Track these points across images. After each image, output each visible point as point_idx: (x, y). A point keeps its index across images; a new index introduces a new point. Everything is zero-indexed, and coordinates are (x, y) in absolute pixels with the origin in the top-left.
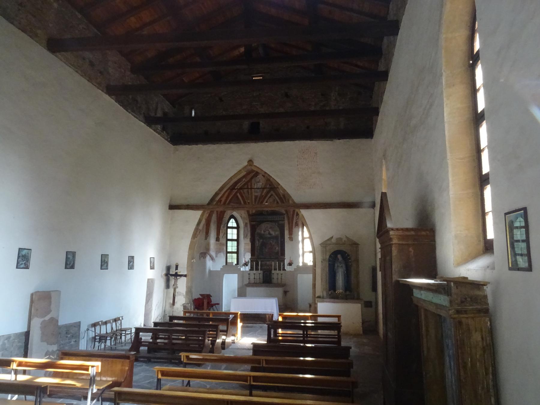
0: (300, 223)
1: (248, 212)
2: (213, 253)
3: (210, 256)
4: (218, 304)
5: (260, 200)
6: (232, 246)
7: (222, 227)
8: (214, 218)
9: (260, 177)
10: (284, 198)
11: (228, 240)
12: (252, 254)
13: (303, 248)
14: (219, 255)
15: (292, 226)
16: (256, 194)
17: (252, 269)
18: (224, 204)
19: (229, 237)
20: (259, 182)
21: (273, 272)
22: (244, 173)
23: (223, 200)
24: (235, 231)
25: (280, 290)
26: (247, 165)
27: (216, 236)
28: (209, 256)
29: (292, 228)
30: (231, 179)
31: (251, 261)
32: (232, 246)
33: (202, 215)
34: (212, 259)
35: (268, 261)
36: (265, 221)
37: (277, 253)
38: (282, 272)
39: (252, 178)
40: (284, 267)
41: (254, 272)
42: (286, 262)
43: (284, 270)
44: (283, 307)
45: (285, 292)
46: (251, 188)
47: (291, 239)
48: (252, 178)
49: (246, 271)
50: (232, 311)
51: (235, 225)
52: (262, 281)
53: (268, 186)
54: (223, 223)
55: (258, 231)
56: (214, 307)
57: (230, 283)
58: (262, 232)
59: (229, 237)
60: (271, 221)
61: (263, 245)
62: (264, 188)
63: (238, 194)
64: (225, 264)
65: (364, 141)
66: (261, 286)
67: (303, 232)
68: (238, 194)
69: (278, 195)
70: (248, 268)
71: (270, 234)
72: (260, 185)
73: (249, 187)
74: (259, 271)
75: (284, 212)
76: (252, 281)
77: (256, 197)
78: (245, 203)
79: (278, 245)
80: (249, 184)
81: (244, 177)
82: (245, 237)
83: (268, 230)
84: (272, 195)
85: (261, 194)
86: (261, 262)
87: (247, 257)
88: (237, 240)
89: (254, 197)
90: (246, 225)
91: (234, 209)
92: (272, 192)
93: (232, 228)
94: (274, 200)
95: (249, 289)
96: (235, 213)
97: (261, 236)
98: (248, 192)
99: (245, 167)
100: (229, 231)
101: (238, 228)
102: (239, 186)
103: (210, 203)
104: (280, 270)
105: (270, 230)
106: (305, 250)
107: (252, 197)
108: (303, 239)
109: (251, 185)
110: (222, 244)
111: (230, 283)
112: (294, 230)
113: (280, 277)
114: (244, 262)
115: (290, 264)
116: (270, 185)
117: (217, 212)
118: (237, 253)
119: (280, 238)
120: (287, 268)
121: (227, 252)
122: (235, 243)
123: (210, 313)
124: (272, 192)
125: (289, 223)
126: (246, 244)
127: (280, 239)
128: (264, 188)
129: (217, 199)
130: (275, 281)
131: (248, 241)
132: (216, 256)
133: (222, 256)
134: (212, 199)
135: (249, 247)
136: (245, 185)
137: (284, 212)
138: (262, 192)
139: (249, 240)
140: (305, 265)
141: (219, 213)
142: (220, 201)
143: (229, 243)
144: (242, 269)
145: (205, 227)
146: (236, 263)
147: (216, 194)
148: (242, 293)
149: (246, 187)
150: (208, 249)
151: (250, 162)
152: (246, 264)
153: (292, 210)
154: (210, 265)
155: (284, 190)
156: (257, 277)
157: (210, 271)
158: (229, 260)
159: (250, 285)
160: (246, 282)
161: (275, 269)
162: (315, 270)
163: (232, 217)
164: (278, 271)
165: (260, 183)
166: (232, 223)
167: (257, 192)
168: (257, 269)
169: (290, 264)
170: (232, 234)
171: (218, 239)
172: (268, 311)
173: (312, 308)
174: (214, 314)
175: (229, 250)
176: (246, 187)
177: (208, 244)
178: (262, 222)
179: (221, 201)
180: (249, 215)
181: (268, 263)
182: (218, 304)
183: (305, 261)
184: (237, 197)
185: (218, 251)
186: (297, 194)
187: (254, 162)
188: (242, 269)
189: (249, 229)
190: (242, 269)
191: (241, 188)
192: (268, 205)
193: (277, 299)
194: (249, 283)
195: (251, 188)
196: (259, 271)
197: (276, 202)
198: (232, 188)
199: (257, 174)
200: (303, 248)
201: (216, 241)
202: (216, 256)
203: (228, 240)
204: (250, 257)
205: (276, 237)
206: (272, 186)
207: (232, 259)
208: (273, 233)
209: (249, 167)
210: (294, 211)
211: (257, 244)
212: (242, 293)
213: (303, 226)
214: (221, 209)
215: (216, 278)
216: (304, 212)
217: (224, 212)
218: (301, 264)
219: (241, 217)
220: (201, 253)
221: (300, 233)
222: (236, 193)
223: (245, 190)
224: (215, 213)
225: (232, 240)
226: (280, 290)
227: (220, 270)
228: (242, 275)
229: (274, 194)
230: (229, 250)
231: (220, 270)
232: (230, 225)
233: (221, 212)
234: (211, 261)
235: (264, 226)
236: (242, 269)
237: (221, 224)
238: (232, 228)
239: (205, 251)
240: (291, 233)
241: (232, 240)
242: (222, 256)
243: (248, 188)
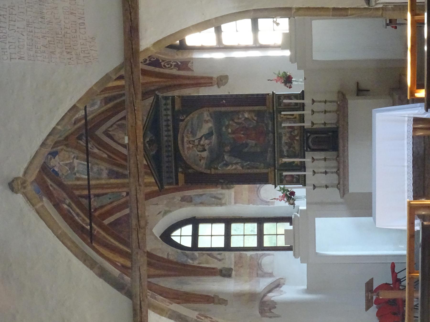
0: (180, 56)
1: (149, 196)
2: (262, 285)
3: (270, 291)
4: (393, 266)
5: (118, 163)
6: (244, 236)
7: (192, 263)
8: (169, 283)
9: (56, 163)
10: (112, 99)
11: (227, 247)
12: (263, 179)
13: (247, 48)
14: (268, 269)
15: (188, 78)
16: (105, 174)
17: (301, 181)
18: (128, 256)
19: (220, 243)
20: (72, 168)
21: (307, 125)
22: (46, 203)
23: (121, 260)
24: (203, 228)
25: (355, 105)
26: (25, 195)
27: (219, 278)
28: (270, 295)
29: (195, 78)
30: (61, 237)
31: (281, 183)
32: (244, 236)
33: (161, 311)
34: (277, 285)
35: (280, 138)
36: (176, 149)
37: (259, 114)
38: (307, 101)
39: (61, 185)
40: (296, 96)
41: (308, 173)
42: (281, 90)
43: (302, 96)
44: (396, 97)
45: (360, 91)
46: (89, 187)
47: (222, 80)
48: (61, 185)
49: (307, 197)
50: (404, 225)
51: (188, 229)
52: (330, 154)
53: (82, 143)
54: (183, 259)
55: (202, 166)
56: (399, 276)
57: (339, 237)
58: (205, 154)
59: (220, 243)
60: (176, 130)
61: (238, 152)
62: (88, 153)
63: (106, 222)
64: (291, 253)
65: (160, 235)
66: (346, 150)
67: (202, 49)
68: (106, 222)
69: (105, 116)
70: (300, 191)
71: (209, 135)
72: (80, 165)
73: (86, 192)
74: (308, 160)
75: (151, 100)
76: (333, 178)
77: (112, 174)
78: (125, 205)
79: (238, 112)
80: (77, 193)
81: (57, 206)
82: (218, 201)
83: (198, 138)
84: (106, 133)
85: (102, 159)
86: (284, 157)
87: (270, 195)
88: (228, 222)
89: (112, 181)
90: (188, 200)
91: (142, 226)
92: (99, 133)
93: (195, 236)
94: (121, 126)
95: (354, 187)
96: (158, 229)
97: (216, 158)
98: (98, 196)
99: (29, 200)
100: (203, 243)
101: (195, 222)
102: (82, 219)
103: (129, 295)
104: (302, 107)
105: (199, 135)
106: (250, 43)
107: (112, 186)
108: (221, 48)
109: (79, 187)
110: (239, 262)
111: (339, 237)
112: (198, 71)
113: (321, 107)
114: (284, 204)
115: (287, 80)
116: (79, 138)
117: (149, 277)
118: (260, 221)
119: (218, 109)
120: (297, 87)
121: (260, 247)
122: (236, 228)
123: (411, 279)
124: (99, 133)
125: (180, 86)
126: (238, 199)
127: (223, 109)
128: (88, 153)
129: (116, 272)
130: (330, 119)
131: (230, 193)
132: (271, 275)
133: (268, 260)
134: (119, 286)
135: (244, 189)
136: (79, 205)
137: (151, 100)
138: (102, 159)
139: (225, 191)
140: (290, 41)
141: (153, 271)
142: (124, 268)
143: (235, 242)
144: (303, 207)
145: (192, 305)
146: (287, 226)
147: (103, 274)
148: (362, 206)
149: (85, 202)
150: (252, 297)
151: (13, 186)
152: (290, 197)
153: (143, 79)
154: (293, 290)
155: (90, 93)
156: (321, 165)
157: (309, 291)
158: (281, 242)
159: (342, 185)
160: (334, 194)
161: (302, 119)
162: (299, 9)
163: (166, 236)
164: (307, 112)
165: (71, 165)
166: (183, 236)
167: (100, 172)
168: (302, 167)
169: (287, 80)
170: (211, 236)
171: (226, 273)
172: (406, 131)
173: (394, 15)
174: (412, 269)
175: (253, 242)
176: (85, 202)
177: (239, 296)
178: (178, 156)
179: (123, 266)
180: (161, 191)
181: (285, 139)
182: (393, 266)
183: (279, 41)
184: (110, 224)
185: (257, 270)
186: (103, 59)
187: (15, 175)
188: (303, 207)
189: (200, 191)
190: (301, 205)
191: (90, 216)
192: (129, 138)
193: (374, 110)
194: (338, 186)
195: (89, 187)
196: (308, 160)
197: (123, 122)
198: (89, 237)
199: (45, 169)
200: (247, 48)
201: (229, 276)
202: (271, 275)
203: (227, 247)
204: (269, 187)
205: (218, 118)
206: (84, 132)
207: (275, 235)
208: (206, 128)
209: (30, 188)
210: (144, 73)
211: (235, 167)
212: (362, 206)
213: (182, 47)
214: (142, 260)
215: (325, 273)
216: (148, 40)
217: (150, 255)
218: (287, 53)
219: (166, 213)
220: (262, 312)
221: (206, 55)
222: (101, 226)
223: (95, 203)
224: (153, 280)
225: (228, 235)
226: (355, 105)
227: (305, 265)
228: (319, 207)
229: (104, 128)
230: (253, 242)
231: (305, 265)
232: (187, 242)
233: (149, 264)
234: (284, 288)
235: (189, 152)
236: (301, 205)
237: (185, 265)
238: (195, 236)
239: (257, 304)
240: (207, 81)
241: (228, 235)
242: (268, 260)
243: (89, 197)
